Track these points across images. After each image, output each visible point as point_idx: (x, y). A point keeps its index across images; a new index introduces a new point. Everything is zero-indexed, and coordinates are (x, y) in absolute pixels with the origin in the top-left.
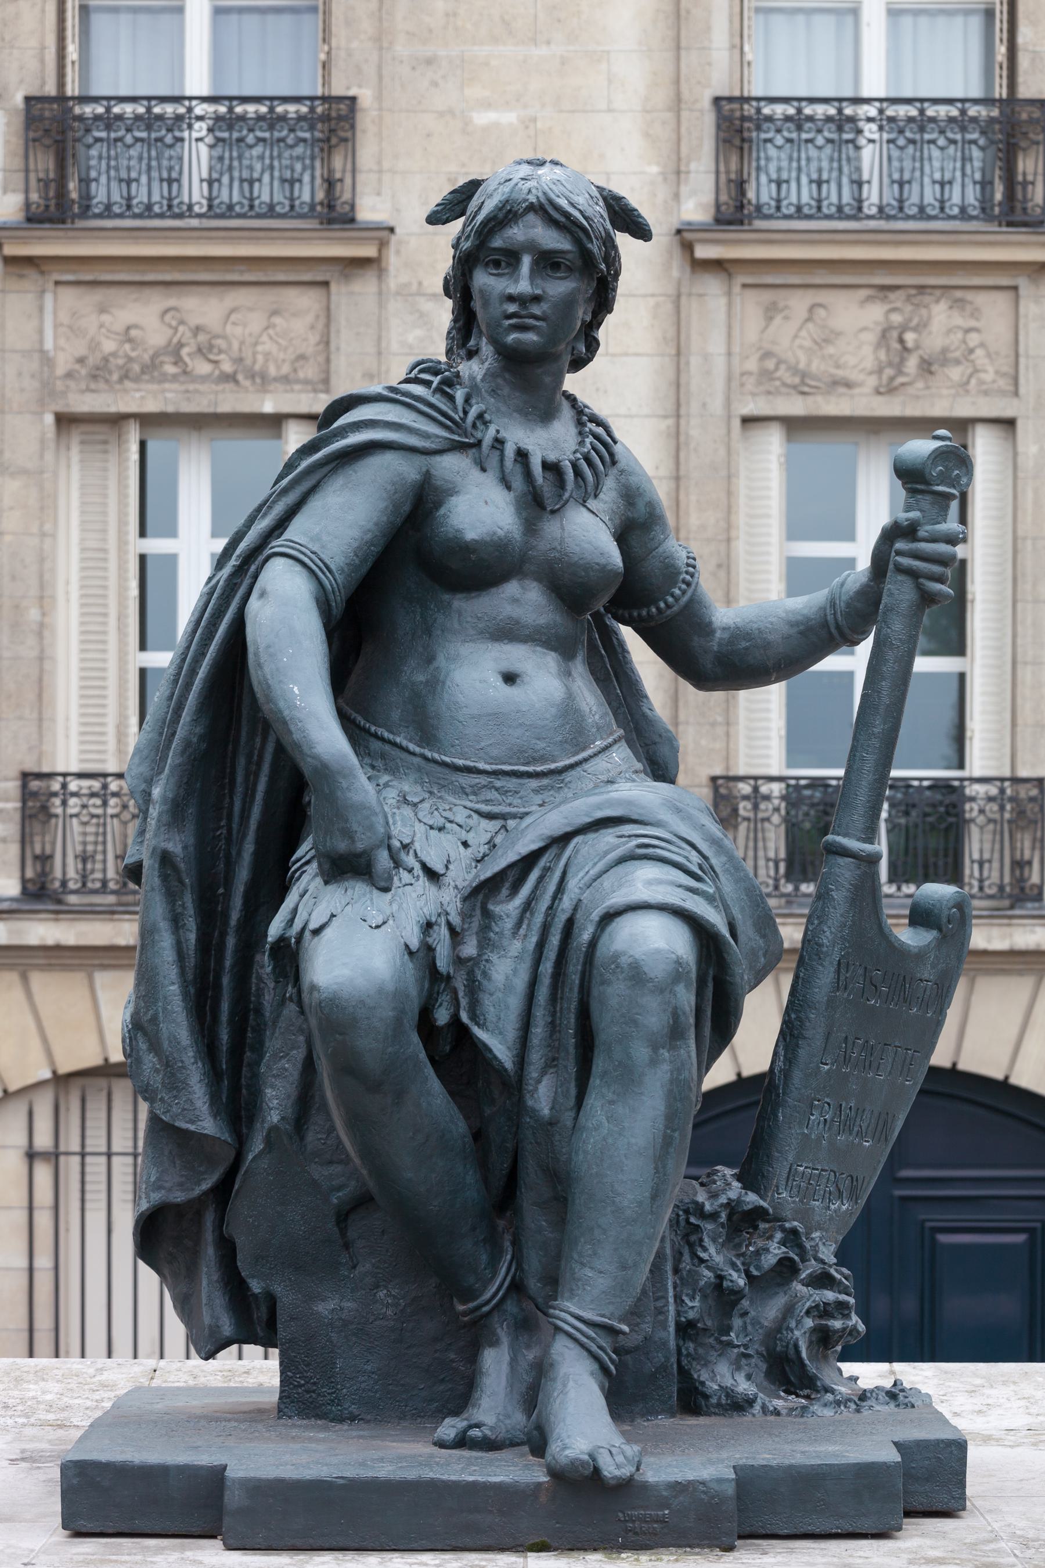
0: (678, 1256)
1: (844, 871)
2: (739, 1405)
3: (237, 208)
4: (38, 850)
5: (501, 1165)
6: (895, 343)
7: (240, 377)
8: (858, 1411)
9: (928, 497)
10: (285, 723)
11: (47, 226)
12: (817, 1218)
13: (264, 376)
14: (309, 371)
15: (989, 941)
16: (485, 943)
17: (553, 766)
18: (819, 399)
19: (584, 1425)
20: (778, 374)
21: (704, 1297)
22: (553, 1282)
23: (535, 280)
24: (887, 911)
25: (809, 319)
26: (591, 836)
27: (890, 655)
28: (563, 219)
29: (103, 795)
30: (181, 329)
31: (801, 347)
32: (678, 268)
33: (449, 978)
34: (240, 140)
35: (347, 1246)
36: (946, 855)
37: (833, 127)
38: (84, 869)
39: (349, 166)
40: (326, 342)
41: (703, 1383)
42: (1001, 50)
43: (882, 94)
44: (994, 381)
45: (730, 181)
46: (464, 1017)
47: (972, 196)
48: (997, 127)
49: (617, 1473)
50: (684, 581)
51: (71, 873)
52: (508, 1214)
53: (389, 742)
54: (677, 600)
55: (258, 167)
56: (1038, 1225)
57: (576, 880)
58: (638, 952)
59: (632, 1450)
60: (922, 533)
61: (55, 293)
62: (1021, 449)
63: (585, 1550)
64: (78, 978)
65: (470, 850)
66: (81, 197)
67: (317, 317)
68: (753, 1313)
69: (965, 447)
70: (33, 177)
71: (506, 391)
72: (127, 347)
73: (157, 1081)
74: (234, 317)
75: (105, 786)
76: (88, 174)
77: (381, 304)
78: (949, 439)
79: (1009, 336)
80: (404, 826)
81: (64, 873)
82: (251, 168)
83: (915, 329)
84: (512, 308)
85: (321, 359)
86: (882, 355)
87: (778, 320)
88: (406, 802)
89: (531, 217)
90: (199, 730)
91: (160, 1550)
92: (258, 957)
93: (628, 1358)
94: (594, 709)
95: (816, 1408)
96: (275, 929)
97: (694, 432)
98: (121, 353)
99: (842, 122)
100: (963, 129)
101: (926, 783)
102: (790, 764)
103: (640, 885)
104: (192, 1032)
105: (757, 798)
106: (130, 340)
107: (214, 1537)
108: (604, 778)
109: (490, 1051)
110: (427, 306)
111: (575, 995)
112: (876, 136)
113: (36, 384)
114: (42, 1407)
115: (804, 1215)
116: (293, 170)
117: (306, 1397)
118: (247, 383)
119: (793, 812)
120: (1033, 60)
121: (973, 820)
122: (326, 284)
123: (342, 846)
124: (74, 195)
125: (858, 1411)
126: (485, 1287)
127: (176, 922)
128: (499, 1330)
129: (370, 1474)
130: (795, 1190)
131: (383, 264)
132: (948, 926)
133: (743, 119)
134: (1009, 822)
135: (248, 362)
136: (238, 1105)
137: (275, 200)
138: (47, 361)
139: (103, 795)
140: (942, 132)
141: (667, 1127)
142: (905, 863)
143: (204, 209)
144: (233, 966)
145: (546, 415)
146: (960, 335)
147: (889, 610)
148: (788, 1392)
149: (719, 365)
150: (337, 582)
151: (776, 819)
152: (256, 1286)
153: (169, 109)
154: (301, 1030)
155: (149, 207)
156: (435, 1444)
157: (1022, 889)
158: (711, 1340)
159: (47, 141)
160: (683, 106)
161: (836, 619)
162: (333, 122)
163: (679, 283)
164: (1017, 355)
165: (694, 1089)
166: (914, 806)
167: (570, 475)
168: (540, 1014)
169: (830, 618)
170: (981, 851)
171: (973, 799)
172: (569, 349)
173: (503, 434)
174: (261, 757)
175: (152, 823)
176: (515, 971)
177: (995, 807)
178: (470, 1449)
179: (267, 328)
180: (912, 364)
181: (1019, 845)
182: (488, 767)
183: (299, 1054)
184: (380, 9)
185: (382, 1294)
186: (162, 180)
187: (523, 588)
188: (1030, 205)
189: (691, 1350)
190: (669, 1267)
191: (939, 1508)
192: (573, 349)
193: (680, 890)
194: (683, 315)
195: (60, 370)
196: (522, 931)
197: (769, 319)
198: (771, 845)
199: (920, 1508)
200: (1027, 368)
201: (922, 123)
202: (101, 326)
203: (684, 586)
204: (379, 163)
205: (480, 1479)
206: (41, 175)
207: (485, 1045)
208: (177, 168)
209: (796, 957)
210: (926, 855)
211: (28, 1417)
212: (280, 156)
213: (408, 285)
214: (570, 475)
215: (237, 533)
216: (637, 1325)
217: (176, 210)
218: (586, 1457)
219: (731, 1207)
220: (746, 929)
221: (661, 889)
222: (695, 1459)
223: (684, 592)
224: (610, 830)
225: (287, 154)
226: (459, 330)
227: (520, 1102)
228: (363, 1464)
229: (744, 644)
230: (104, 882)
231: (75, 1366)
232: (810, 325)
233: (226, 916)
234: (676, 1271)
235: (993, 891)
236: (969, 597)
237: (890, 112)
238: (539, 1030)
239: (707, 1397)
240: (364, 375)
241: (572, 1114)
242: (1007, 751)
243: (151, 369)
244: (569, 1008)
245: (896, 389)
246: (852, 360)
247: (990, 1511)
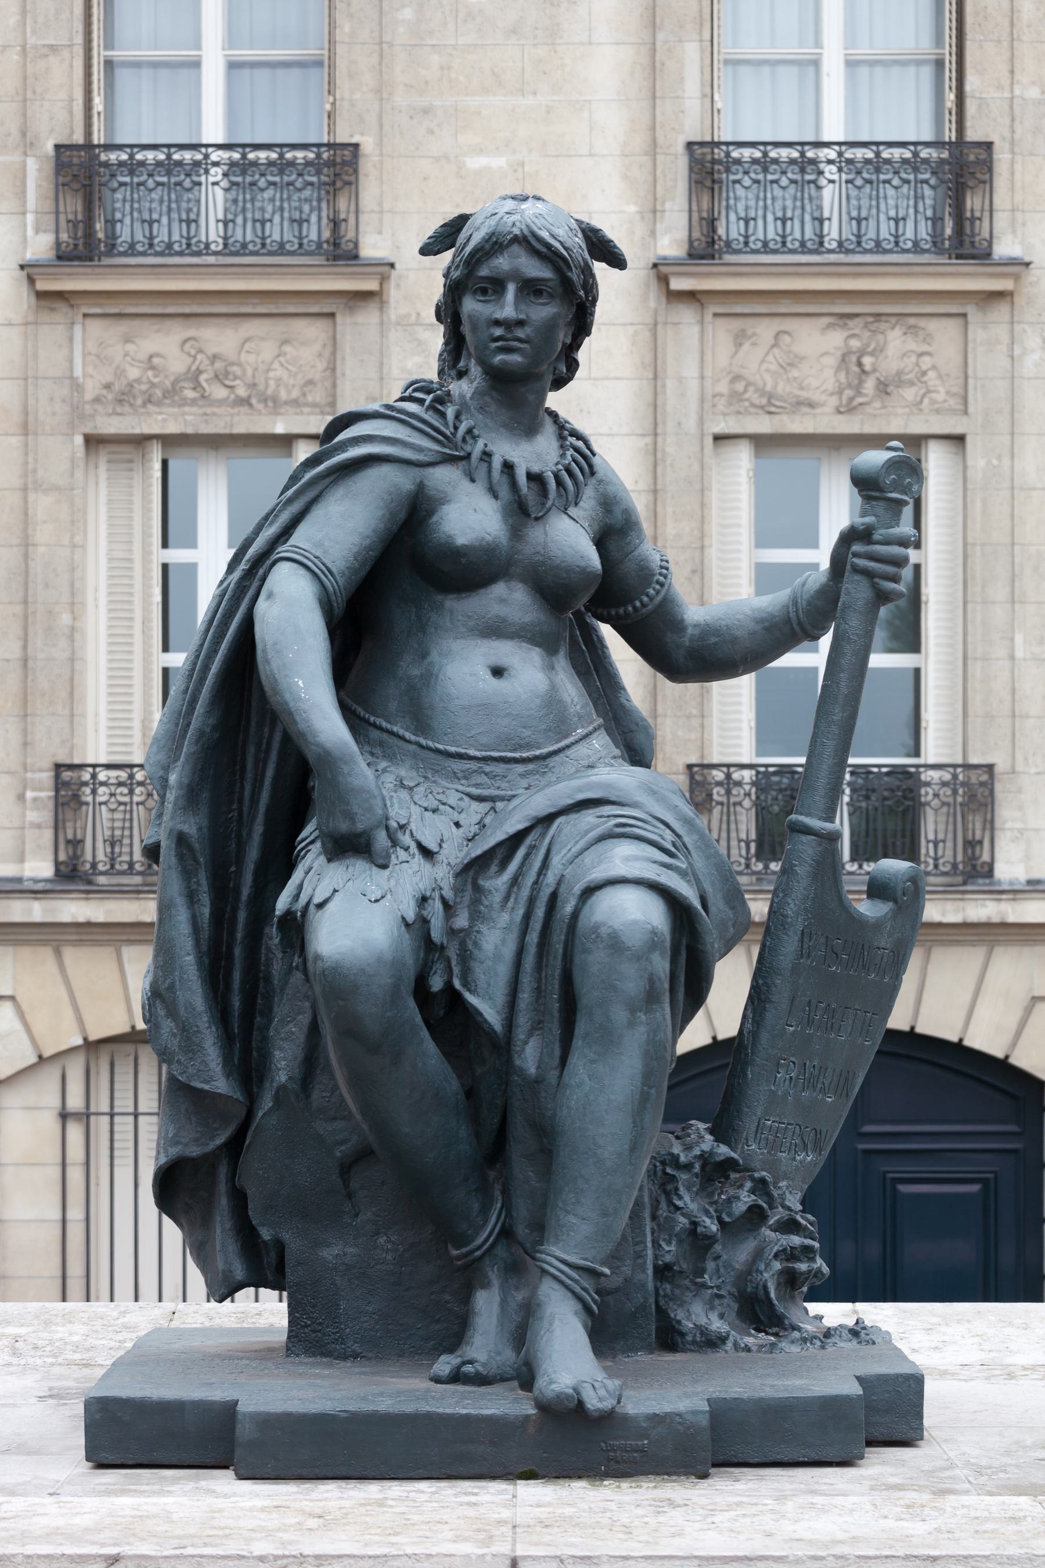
0: (655, 1205)
1: (807, 848)
2: (712, 1342)
3: (251, 247)
4: (70, 836)
6: (854, 366)
7: (254, 401)
8: (823, 1347)
9: (882, 503)
10: (291, 714)
11: (76, 263)
12: (784, 1168)
13: (275, 400)
14: (317, 395)
15: (943, 915)
16: (475, 915)
17: (538, 752)
18: (785, 417)
19: (570, 1362)
20: (747, 396)
21: (680, 1242)
22: (540, 1228)
23: (520, 307)
24: (846, 888)
25: (774, 345)
26: (573, 817)
27: (848, 649)
28: (544, 250)
29: (130, 784)
30: (199, 357)
31: (767, 370)
32: (654, 298)
33: (442, 948)
34: (253, 184)
35: (349, 1196)
36: (904, 836)
37: (796, 168)
38: (113, 853)
39: (353, 207)
40: (332, 368)
41: (679, 1322)
42: (951, 97)
43: (841, 138)
44: (945, 401)
45: (701, 219)
46: (457, 984)
47: (924, 231)
48: (947, 167)
49: (600, 1405)
50: (658, 582)
51: (101, 856)
52: (498, 1165)
53: (387, 731)
54: (651, 599)
55: (269, 208)
56: (991, 1176)
57: (559, 857)
58: (617, 923)
59: (613, 1384)
60: (876, 537)
61: (84, 325)
62: (970, 462)
63: (570, 1478)
64: (106, 953)
65: (461, 830)
66: (107, 237)
67: (324, 345)
68: (725, 1257)
69: (919, 461)
70: (62, 217)
71: (493, 408)
72: (150, 373)
73: (174, 1044)
74: (247, 346)
75: (131, 776)
76: (113, 215)
77: (383, 334)
78: (901, 450)
79: (958, 359)
80: (400, 809)
81: (94, 856)
82: (263, 210)
83: (872, 354)
84: (498, 332)
85: (328, 384)
86: (842, 377)
87: (746, 346)
88: (402, 785)
89: (515, 248)
90: (211, 721)
91: (175, 1481)
92: (267, 930)
93: (610, 1299)
94: (576, 699)
95: (784, 1344)
96: (282, 903)
97: (670, 450)
98: (145, 379)
99: (805, 164)
100: (916, 170)
101: (884, 770)
102: (759, 754)
103: (618, 862)
105: (729, 783)
106: (153, 368)
107: (226, 1467)
108: (585, 763)
109: (481, 1015)
110: (424, 335)
111: (559, 963)
112: (836, 177)
113: (67, 409)
114: (69, 1347)
115: (772, 1165)
116: (301, 212)
118: (260, 406)
119: (762, 797)
120: (980, 106)
121: (928, 804)
122: (332, 315)
123: (344, 827)
124: (101, 235)
125: (823, 1347)
126: (477, 1234)
127: (191, 897)
128: (490, 1273)
129: (371, 1408)
130: (763, 1142)
131: (385, 298)
132: (903, 898)
133: (714, 162)
134: (961, 805)
135: (261, 387)
137: (285, 239)
138: (77, 387)
139: (130, 784)
140: (896, 173)
141: (644, 1084)
142: (866, 843)
143: (220, 248)
144: (244, 938)
145: (530, 430)
146: (913, 359)
147: (846, 607)
148: (758, 1330)
149: (693, 387)
150: (338, 584)
151: (747, 803)
152: (266, 1234)
153: (188, 156)
154: (306, 997)
155: (169, 245)
156: (431, 1379)
157: (974, 867)
158: (687, 1282)
159: (76, 186)
160: (658, 150)
161: (798, 616)
162: (337, 167)
163: (656, 313)
164: (966, 377)
165: (669, 1049)
166: (874, 791)
168: (527, 981)
169: (792, 615)
170: (936, 832)
171: (928, 784)
172: (551, 369)
173: (491, 448)
175: (169, 806)
176: (503, 941)
177: (949, 792)
178: (464, 1383)
179: (278, 356)
180: (870, 386)
181: (970, 826)
182: (478, 754)
183: (305, 1019)
184: (380, 64)
185: (382, 1240)
186: (181, 221)
187: (509, 588)
188: (977, 239)
189: (668, 1291)
190: (647, 1214)
191: (899, 1438)
192: (555, 369)
193: (655, 866)
194: (659, 342)
195: (89, 396)
196: (510, 904)
197: (739, 345)
198: (743, 827)
199: (881, 1438)
200: (975, 388)
201: (878, 164)
202: (126, 355)
203: (658, 587)
204: (380, 204)
205: (472, 1412)
206: (71, 217)
207: (475, 1009)
208: (195, 210)
209: (762, 930)
210: (885, 837)
211: (56, 1357)
212: (289, 199)
213: (408, 315)
215: (246, 540)
216: (618, 1268)
217: (195, 248)
218: (571, 1391)
219: (704, 1157)
220: (717, 902)
221: (638, 864)
222: (671, 1392)
223: (658, 592)
224: (591, 811)
225: (295, 197)
226: (450, 352)
227: (509, 1061)
228: (364, 1399)
229: (713, 640)
230: (131, 864)
231: (100, 1309)
232: (776, 351)
233: (237, 891)
234: (654, 1217)
235: (947, 868)
236: (923, 598)
237: (848, 155)
238: (526, 996)
239: (683, 1335)
240: (367, 399)
241: (557, 1072)
242: (959, 739)
243: (172, 394)
244: (553, 975)
245: (855, 408)
246: (814, 383)
247: (946, 1441)
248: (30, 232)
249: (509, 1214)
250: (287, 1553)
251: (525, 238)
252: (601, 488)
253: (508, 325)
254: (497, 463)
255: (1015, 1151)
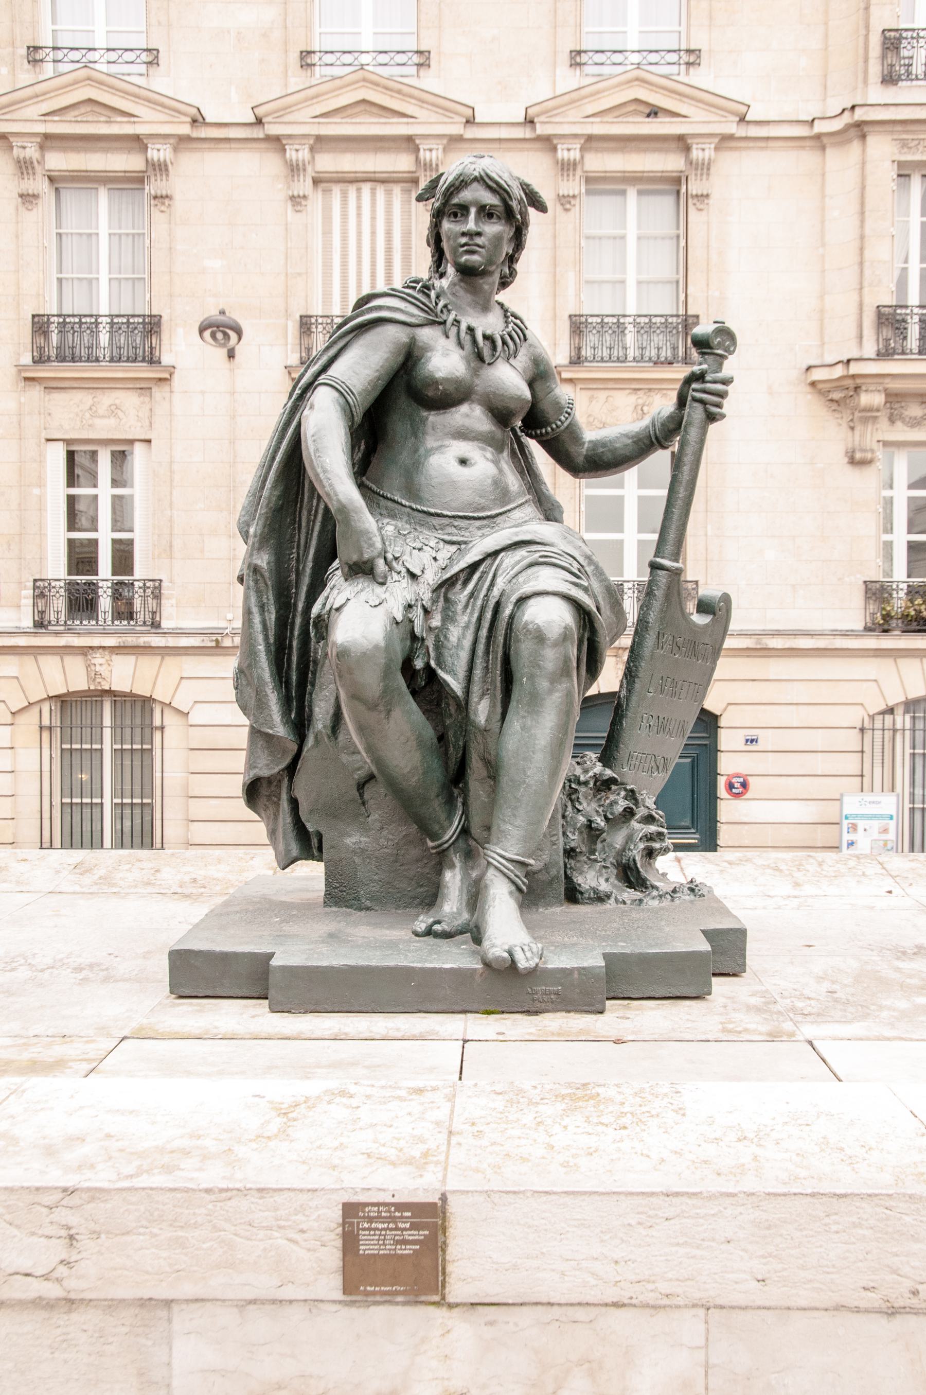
2: (600, 898)
5: (454, 755)
9: (712, 357)
17: (489, 513)
19: (506, 928)
21: (581, 833)
28: (494, 186)
35: (364, 803)
41: (579, 885)
46: (433, 663)
53: (391, 500)
59: (537, 947)
60: (708, 378)
68: (608, 840)
84: (464, 240)
86: (635, 415)
87: (594, 402)
89: (475, 185)
90: (277, 493)
96: (315, 610)
99: (619, 324)
104: (271, 676)
109: (448, 685)
117: (341, 894)
127: (262, 608)
136: (300, 725)
144: (299, 635)
145: (485, 308)
152: (310, 828)
158: (585, 858)
161: (655, 434)
167: (499, 343)
172: (499, 270)
174: (316, 511)
182: (449, 513)
185: (385, 833)
190: (560, 816)
196: (468, 611)
205: (437, 966)
207: (445, 681)
214: (499, 343)
229: (601, 450)
233: (295, 605)
234: (564, 817)
239: (582, 893)
248: (289, 353)
249: (467, 819)
250: (231, 1186)
251: (481, 177)
252: (532, 349)
253: (471, 235)
254: (463, 327)
255: (706, 745)
